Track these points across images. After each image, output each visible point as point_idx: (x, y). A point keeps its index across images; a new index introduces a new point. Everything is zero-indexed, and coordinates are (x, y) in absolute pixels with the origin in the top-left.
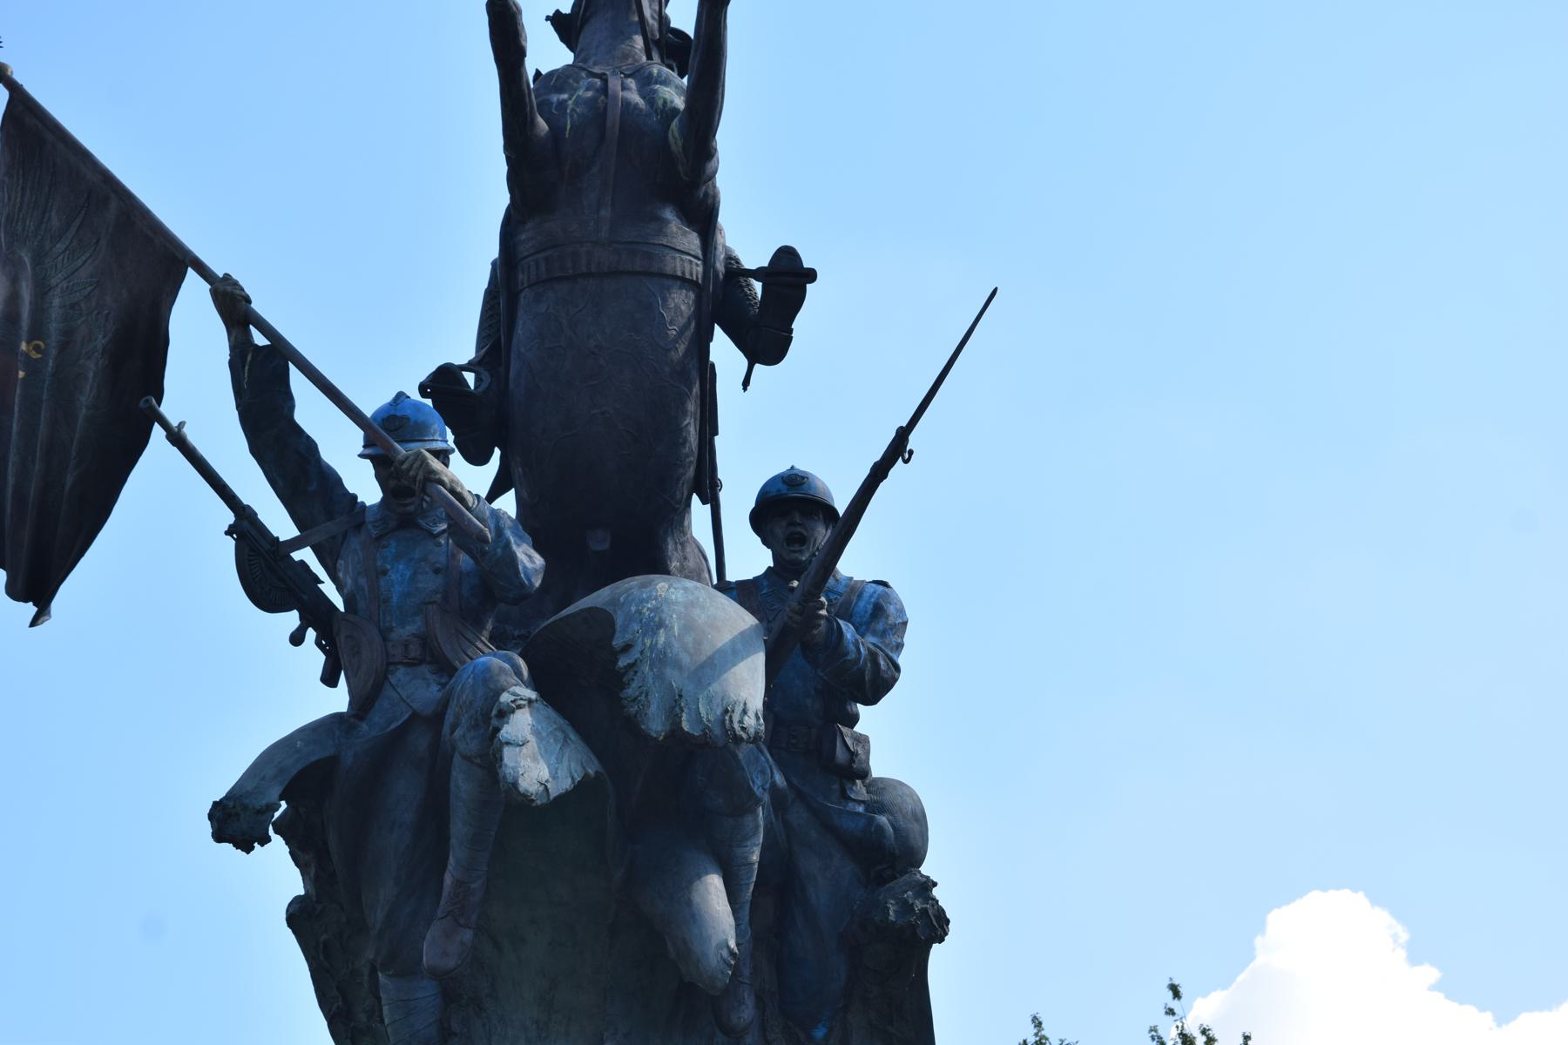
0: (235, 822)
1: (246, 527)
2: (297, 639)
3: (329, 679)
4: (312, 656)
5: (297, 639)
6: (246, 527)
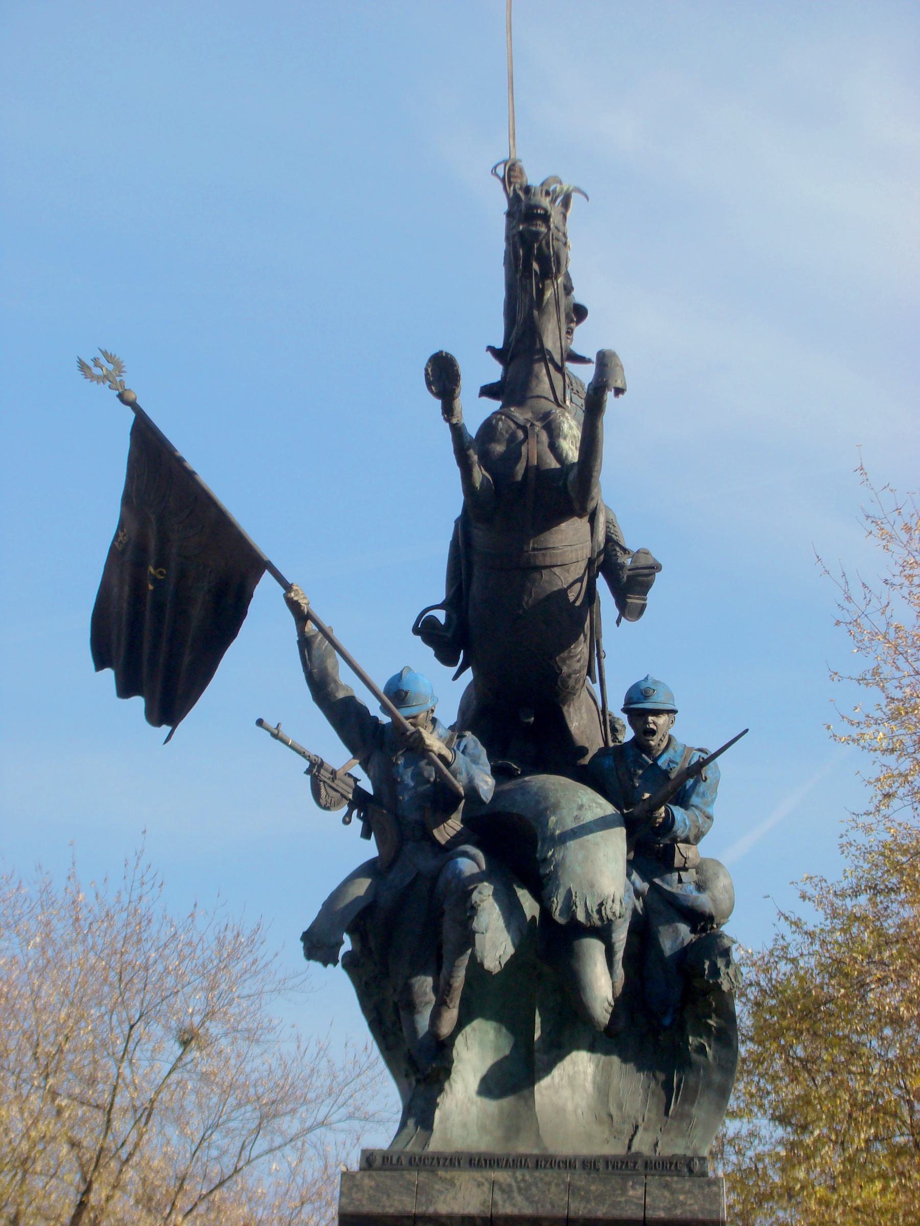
0: (317, 945)
1: (316, 768)
2: (347, 820)
3: (366, 834)
4: (357, 824)
5: (347, 820)
6: (316, 768)
